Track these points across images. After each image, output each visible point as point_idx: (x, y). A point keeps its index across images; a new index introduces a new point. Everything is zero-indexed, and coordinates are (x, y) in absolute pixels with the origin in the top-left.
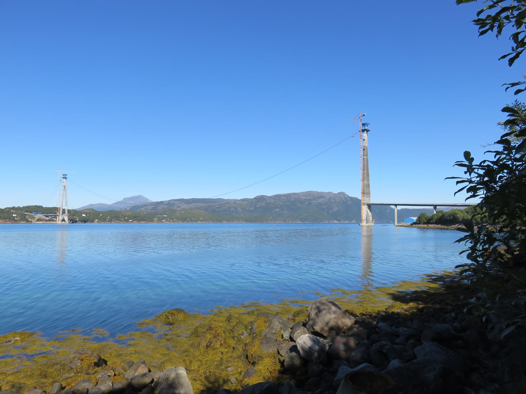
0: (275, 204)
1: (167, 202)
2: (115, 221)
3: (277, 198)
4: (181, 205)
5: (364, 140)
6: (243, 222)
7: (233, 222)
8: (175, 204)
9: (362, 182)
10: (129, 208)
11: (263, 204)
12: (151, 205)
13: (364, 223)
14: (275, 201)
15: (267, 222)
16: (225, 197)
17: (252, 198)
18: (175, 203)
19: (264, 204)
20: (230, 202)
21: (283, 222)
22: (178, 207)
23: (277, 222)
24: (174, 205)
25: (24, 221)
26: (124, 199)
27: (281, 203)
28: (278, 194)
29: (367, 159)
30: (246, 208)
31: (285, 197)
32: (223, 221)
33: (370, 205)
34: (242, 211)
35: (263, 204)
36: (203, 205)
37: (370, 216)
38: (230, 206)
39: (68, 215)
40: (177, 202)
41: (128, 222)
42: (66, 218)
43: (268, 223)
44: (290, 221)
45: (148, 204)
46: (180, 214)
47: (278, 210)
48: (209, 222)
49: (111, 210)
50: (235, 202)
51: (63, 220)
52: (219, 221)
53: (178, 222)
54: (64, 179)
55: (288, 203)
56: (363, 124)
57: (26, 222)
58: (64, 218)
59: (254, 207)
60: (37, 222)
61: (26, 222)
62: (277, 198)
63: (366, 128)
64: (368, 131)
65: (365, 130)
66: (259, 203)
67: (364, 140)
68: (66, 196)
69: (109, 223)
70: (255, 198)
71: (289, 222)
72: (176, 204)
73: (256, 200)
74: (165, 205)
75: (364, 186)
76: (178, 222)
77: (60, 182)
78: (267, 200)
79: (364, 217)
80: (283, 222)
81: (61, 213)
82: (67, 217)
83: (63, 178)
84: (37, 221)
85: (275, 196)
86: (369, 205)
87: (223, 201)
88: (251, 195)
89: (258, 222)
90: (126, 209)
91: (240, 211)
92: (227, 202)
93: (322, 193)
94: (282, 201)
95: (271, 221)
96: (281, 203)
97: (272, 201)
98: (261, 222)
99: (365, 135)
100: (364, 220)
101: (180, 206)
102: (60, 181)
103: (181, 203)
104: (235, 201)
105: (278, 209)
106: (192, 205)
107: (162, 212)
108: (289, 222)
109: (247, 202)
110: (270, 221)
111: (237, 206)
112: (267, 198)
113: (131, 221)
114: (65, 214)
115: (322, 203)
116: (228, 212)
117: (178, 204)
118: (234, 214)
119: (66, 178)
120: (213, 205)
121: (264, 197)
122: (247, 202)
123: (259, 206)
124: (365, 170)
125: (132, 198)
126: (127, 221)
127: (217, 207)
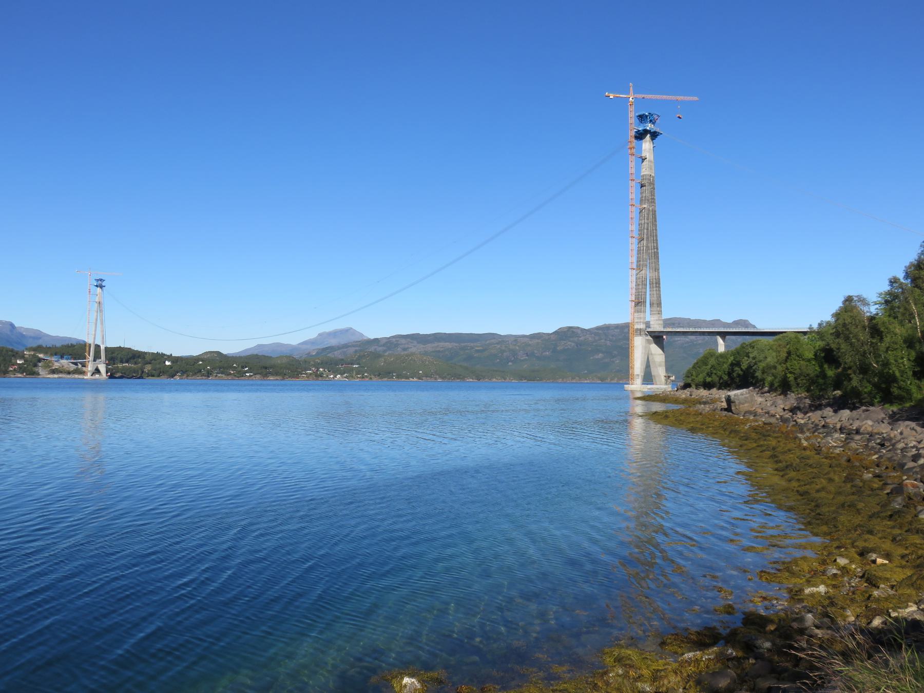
0: (594, 344)
1: (385, 341)
2: (216, 376)
3: (600, 332)
4: (410, 346)
5: (643, 159)
6: (513, 381)
7: (490, 380)
8: (399, 345)
9: (634, 272)
10: (316, 351)
11: (570, 343)
12: (354, 346)
13: (637, 386)
14: (597, 338)
15: (565, 380)
16: (502, 331)
17: (551, 332)
18: (399, 342)
19: (573, 344)
20: (507, 340)
21: (600, 382)
22: (405, 349)
23: (586, 382)
24: (397, 345)
25: (22, 373)
26: (320, 335)
27: (608, 343)
28: (607, 324)
29: (654, 212)
30: (536, 351)
31: (618, 330)
32: (466, 379)
33: (661, 334)
34: (527, 358)
35: (570, 344)
36: (448, 345)
37: (660, 366)
38: (503, 348)
39: (107, 362)
40: (403, 341)
41: (243, 378)
42: (102, 368)
43: (565, 383)
44: (616, 379)
45: (350, 344)
46: (384, 362)
47: (601, 355)
48: (436, 379)
49: (255, 353)
50: (515, 340)
51: (97, 371)
52: (458, 378)
53: (371, 378)
54: (99, 289)
55: (624, 342)
56: (642, 118)
57: (26, 375)
58: (97, 367)
59: (551, 350)
60: (49, 376)
61: (26, 375)
62: (600, 332)
63: (649, 126)
64: (654, 135)
65: (646, 132)
66: (563, 342)
67: (643, 159)
68: (102, 324)
69: (202, 379)
70: (556, 333)
71: (613, 382)
72: (402, 344)
73: (556, 336)
74: (380, 346)
75: (641, 284)
76: (371, 378)
77: (90, 294)
78: (580, 337)
79: (638, 367)
80: (600, 382)
81: (91, 358)
82: (105, 365)
83: (97, 286)
84: (49, 374)
85: (598, 328)
86: (656, 334)
87: (494, 338)
88: (549, 327)
89: (545, 381)
90: (311, 354)
91: (522, 359)
92: (500, 340)
93: (698, 322)
94: (611, 337)
95: (573, 379)
96: (608, 343)
97: (590, 339)
98: (551, 381)
99: (647, 145)
100: (638, 375)
101: (408, 348)
102: (90, 292)
103: (412, 343)
104: (516, 339)
105: (600, 354)
106: (429, 347)
107: (355, 359)
108: (613, 382)
109: (539, 341)
110: (570, 378)
111: (517, 348)
112: (579, 332)
113: (250, 376)
114: (100, 360)
115: (695, 343)
116: (498, 360)
117: (405, 344)
118: (510, 364)
119: (101, 287)
120: (468, 346)
121: (574, 330)
122: (539, 341)
123: (562, 348)
124: (643, 239)
125: (334, 334)
126: (240, 374)
127: (476, 350)
